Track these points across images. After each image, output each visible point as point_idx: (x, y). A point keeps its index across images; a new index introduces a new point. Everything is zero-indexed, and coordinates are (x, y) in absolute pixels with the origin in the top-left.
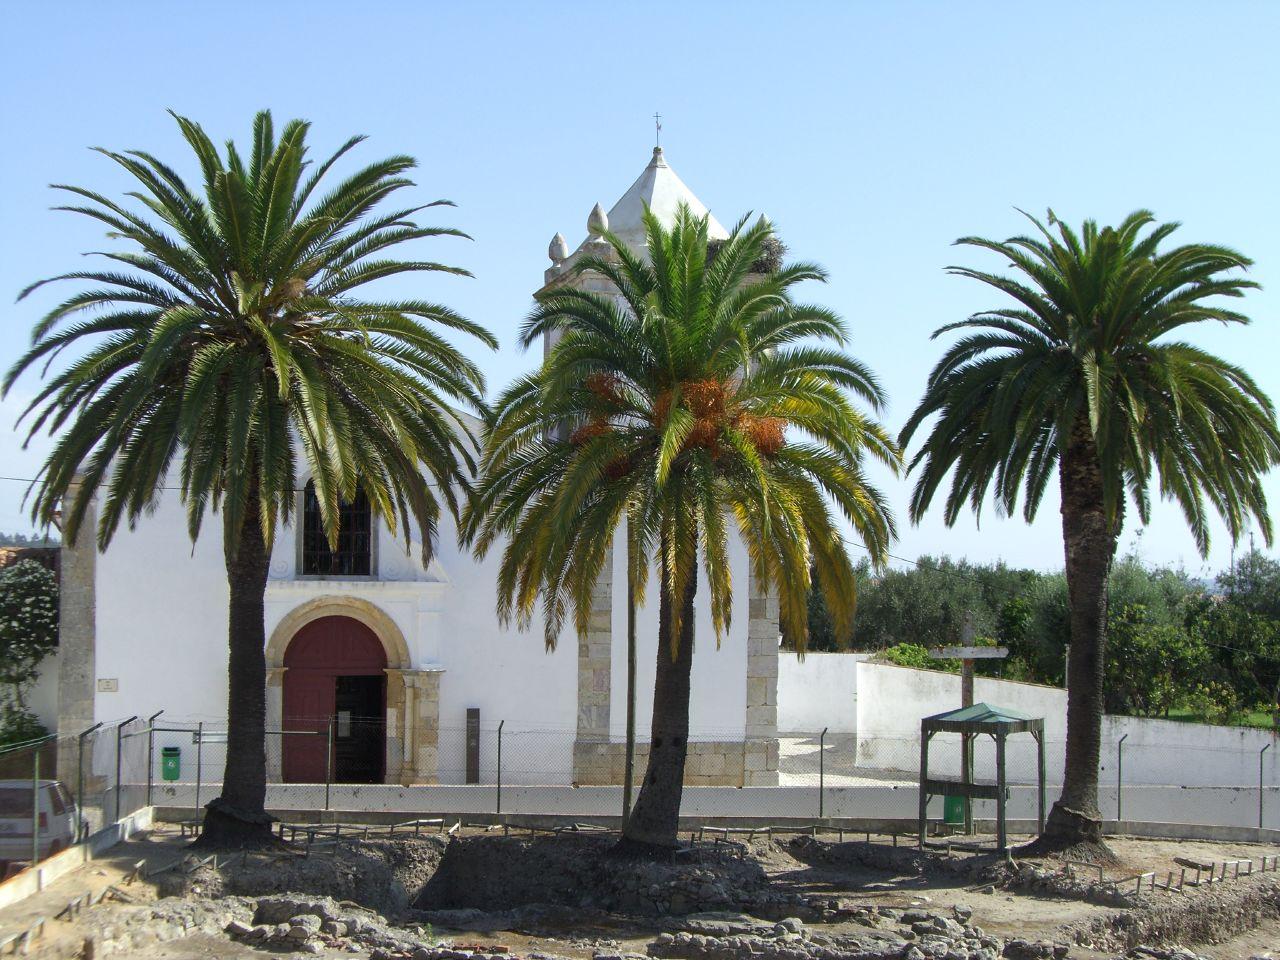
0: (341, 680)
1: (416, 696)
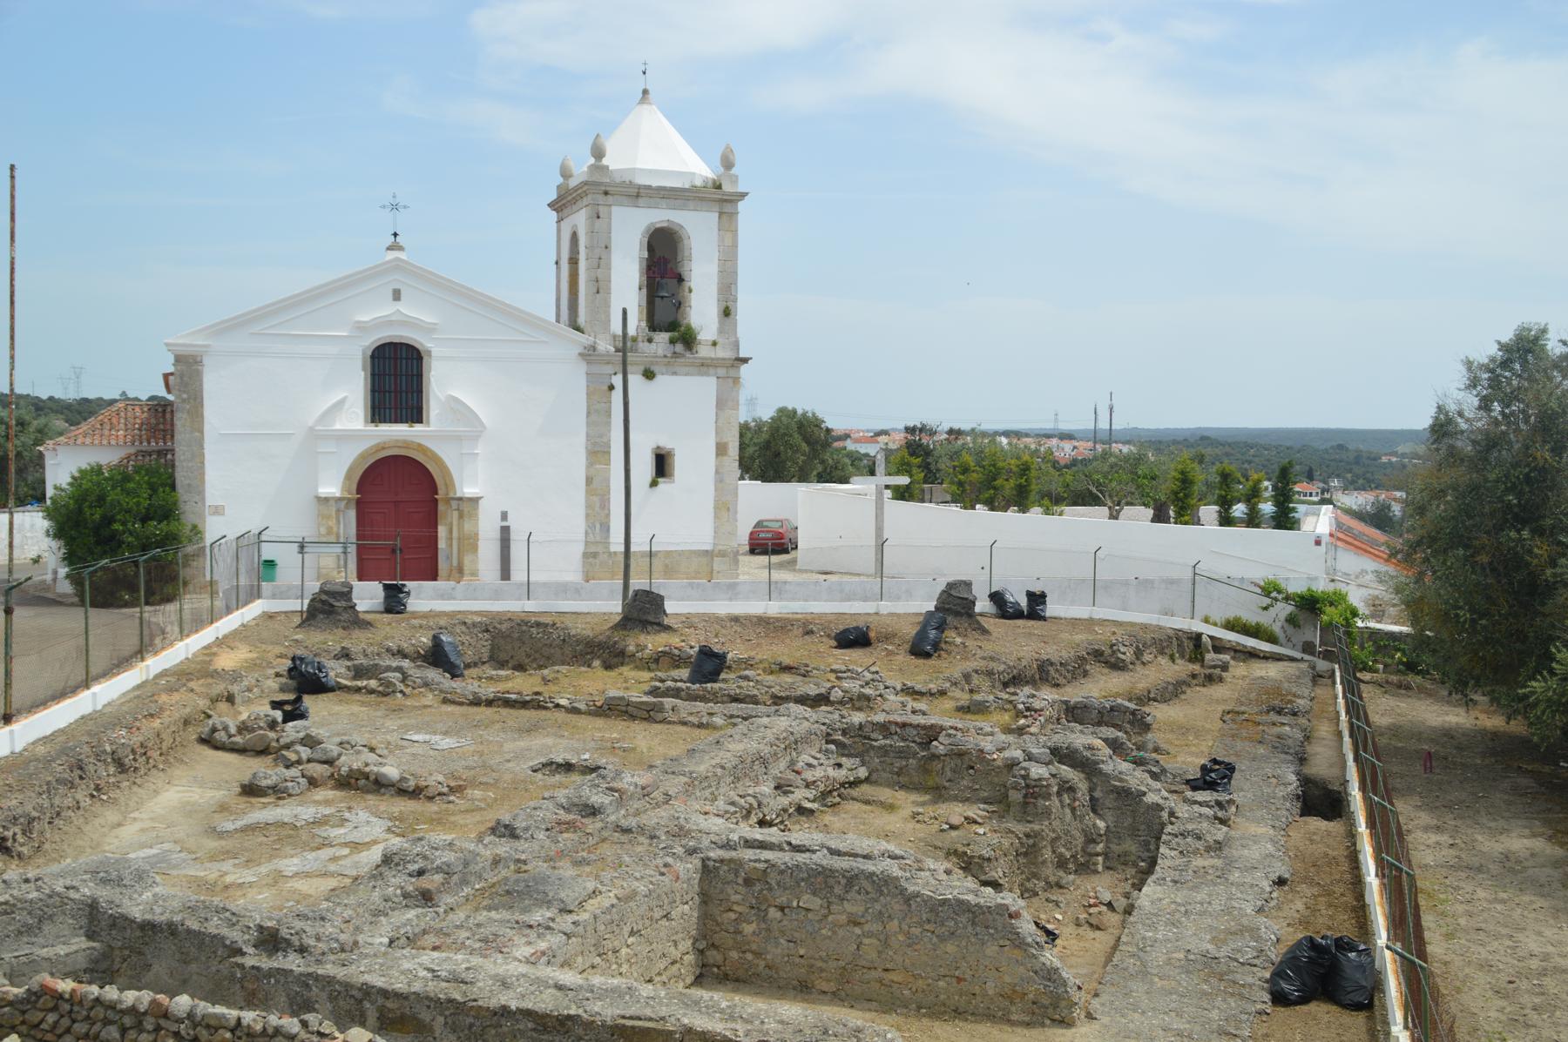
0: (223, 514)
1: (461, 516)
